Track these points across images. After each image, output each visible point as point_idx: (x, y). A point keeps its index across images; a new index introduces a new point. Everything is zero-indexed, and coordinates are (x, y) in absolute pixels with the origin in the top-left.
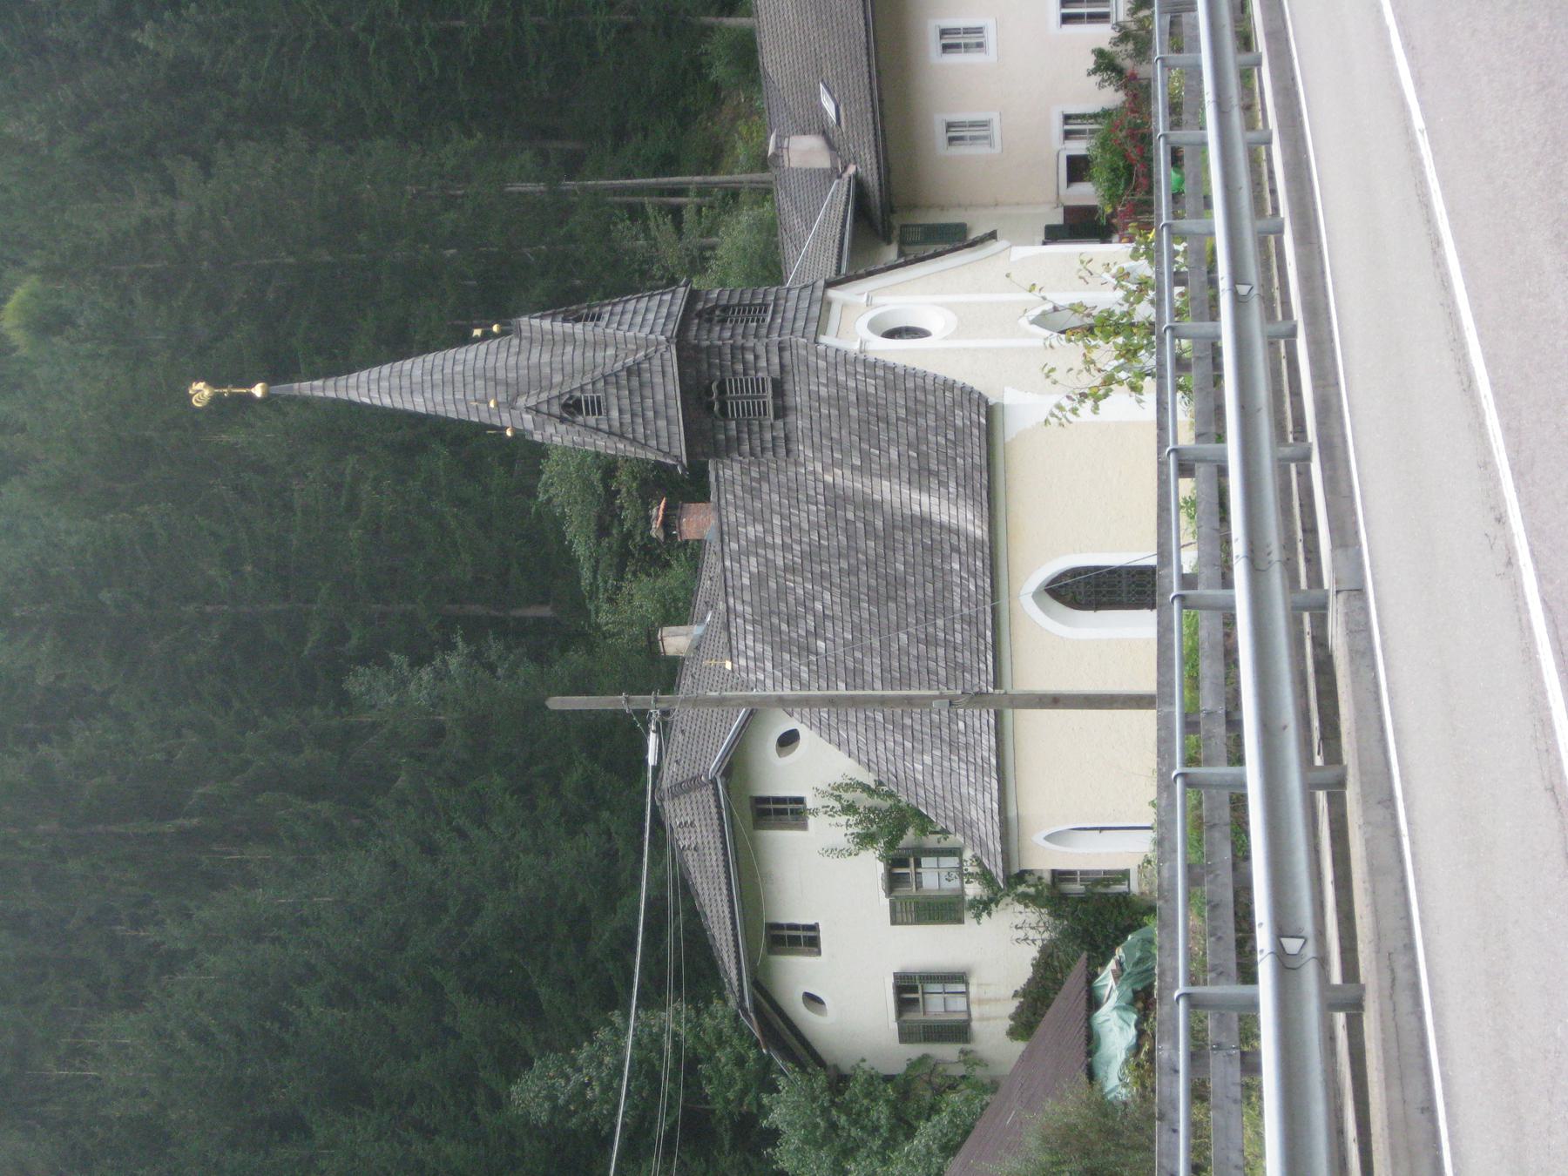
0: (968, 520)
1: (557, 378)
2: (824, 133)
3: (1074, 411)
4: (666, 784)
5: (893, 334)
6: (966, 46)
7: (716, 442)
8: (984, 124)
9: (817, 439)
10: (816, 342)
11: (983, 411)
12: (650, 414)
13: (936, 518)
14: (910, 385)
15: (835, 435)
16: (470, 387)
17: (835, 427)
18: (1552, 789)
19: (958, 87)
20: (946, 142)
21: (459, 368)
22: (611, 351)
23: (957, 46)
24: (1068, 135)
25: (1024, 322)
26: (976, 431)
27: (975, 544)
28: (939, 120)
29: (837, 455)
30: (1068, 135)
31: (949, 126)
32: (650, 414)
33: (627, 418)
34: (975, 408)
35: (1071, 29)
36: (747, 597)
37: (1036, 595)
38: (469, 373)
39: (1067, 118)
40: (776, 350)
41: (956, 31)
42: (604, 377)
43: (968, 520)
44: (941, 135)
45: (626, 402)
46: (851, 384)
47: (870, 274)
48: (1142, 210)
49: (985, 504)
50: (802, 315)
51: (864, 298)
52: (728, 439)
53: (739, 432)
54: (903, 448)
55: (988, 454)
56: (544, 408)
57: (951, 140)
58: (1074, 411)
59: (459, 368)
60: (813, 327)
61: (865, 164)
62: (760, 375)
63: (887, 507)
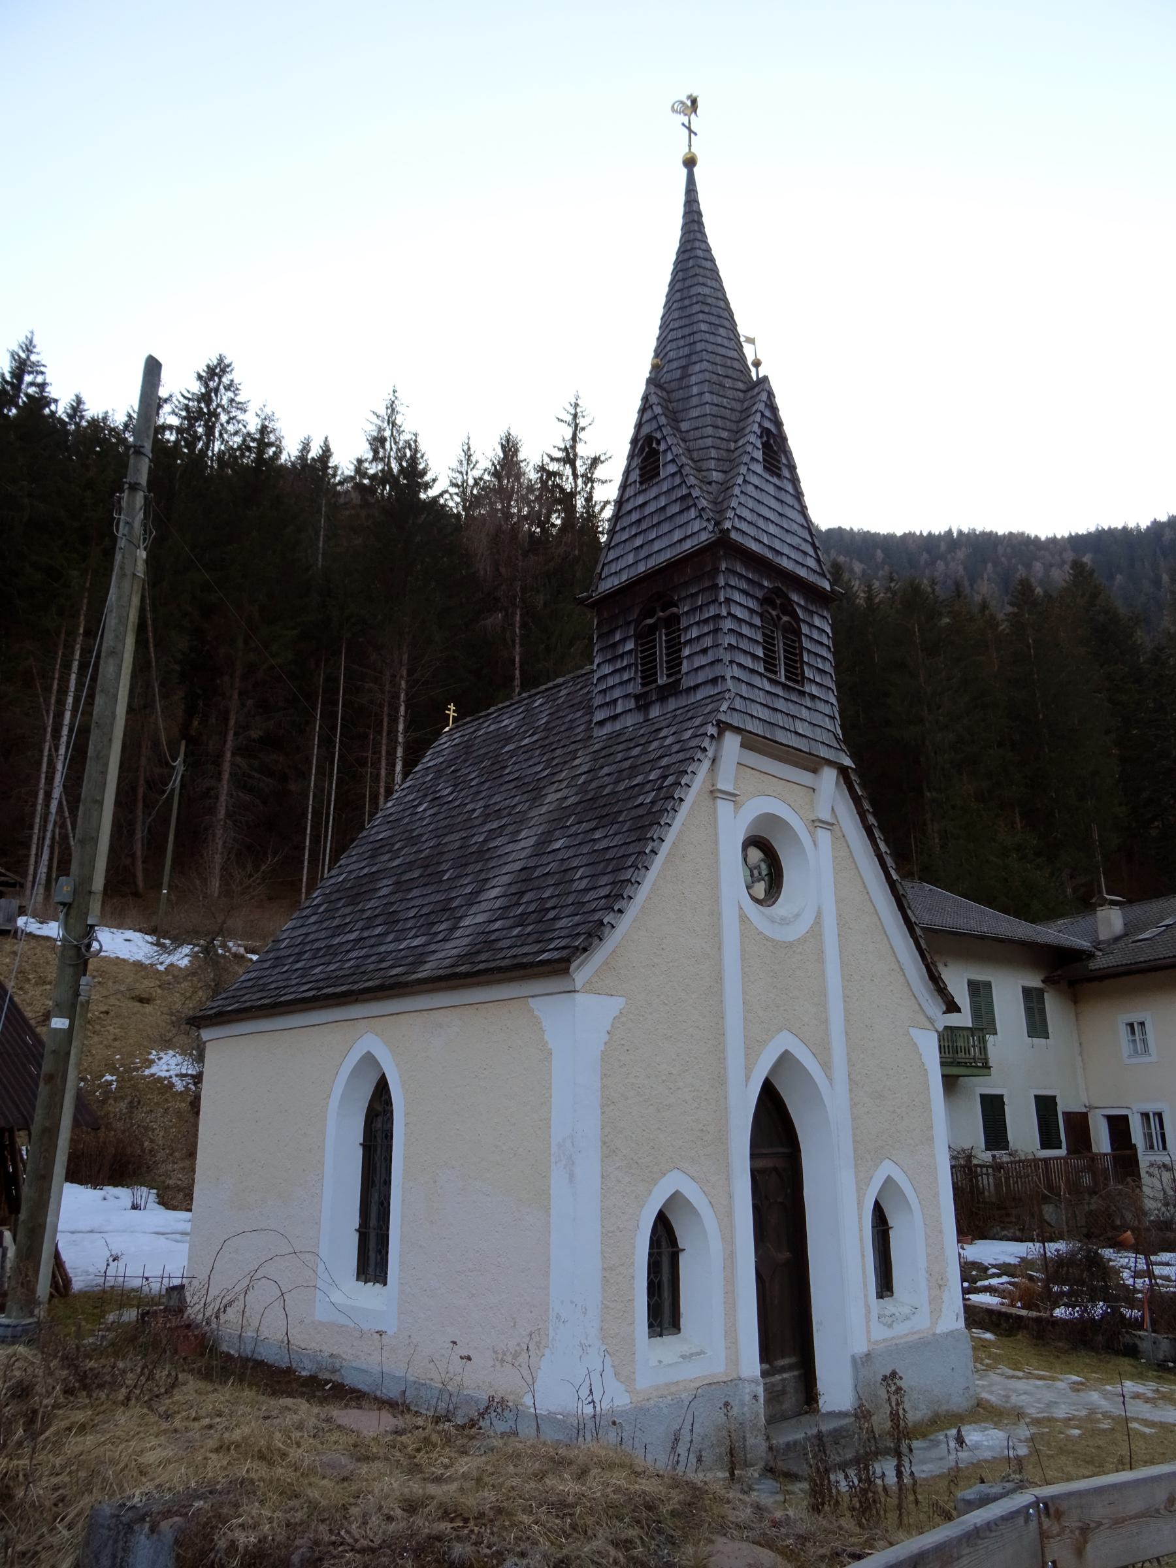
2: (1126, 935)
3: (480, 1428)
4: (104, 649)
6: (1134, 1041)
7: (612, 632)
8: (1146, 1051)
12: (638, 542)
16: (681, 343)
18: (91, 1232)
20: (1130, 1021)
21: (703, 327)
22: (715, 476)
23: (1133, 1033)
24: (1145, 1116)
30: (1145, 1116)
31: (1142, 1024)
32: (638, 542)
33: (635, 516)
36: (492, 728)
39: (1159, 1115)
41: (1144, 1033)
44: (1135, 1017)
51: (826, 816)
52: (614, 645)
53: (622, 656)
55: (500, 969)
57: (1131, 1025)
58: (480, 1428)
60: (751, 726)
61: (1101, 962)
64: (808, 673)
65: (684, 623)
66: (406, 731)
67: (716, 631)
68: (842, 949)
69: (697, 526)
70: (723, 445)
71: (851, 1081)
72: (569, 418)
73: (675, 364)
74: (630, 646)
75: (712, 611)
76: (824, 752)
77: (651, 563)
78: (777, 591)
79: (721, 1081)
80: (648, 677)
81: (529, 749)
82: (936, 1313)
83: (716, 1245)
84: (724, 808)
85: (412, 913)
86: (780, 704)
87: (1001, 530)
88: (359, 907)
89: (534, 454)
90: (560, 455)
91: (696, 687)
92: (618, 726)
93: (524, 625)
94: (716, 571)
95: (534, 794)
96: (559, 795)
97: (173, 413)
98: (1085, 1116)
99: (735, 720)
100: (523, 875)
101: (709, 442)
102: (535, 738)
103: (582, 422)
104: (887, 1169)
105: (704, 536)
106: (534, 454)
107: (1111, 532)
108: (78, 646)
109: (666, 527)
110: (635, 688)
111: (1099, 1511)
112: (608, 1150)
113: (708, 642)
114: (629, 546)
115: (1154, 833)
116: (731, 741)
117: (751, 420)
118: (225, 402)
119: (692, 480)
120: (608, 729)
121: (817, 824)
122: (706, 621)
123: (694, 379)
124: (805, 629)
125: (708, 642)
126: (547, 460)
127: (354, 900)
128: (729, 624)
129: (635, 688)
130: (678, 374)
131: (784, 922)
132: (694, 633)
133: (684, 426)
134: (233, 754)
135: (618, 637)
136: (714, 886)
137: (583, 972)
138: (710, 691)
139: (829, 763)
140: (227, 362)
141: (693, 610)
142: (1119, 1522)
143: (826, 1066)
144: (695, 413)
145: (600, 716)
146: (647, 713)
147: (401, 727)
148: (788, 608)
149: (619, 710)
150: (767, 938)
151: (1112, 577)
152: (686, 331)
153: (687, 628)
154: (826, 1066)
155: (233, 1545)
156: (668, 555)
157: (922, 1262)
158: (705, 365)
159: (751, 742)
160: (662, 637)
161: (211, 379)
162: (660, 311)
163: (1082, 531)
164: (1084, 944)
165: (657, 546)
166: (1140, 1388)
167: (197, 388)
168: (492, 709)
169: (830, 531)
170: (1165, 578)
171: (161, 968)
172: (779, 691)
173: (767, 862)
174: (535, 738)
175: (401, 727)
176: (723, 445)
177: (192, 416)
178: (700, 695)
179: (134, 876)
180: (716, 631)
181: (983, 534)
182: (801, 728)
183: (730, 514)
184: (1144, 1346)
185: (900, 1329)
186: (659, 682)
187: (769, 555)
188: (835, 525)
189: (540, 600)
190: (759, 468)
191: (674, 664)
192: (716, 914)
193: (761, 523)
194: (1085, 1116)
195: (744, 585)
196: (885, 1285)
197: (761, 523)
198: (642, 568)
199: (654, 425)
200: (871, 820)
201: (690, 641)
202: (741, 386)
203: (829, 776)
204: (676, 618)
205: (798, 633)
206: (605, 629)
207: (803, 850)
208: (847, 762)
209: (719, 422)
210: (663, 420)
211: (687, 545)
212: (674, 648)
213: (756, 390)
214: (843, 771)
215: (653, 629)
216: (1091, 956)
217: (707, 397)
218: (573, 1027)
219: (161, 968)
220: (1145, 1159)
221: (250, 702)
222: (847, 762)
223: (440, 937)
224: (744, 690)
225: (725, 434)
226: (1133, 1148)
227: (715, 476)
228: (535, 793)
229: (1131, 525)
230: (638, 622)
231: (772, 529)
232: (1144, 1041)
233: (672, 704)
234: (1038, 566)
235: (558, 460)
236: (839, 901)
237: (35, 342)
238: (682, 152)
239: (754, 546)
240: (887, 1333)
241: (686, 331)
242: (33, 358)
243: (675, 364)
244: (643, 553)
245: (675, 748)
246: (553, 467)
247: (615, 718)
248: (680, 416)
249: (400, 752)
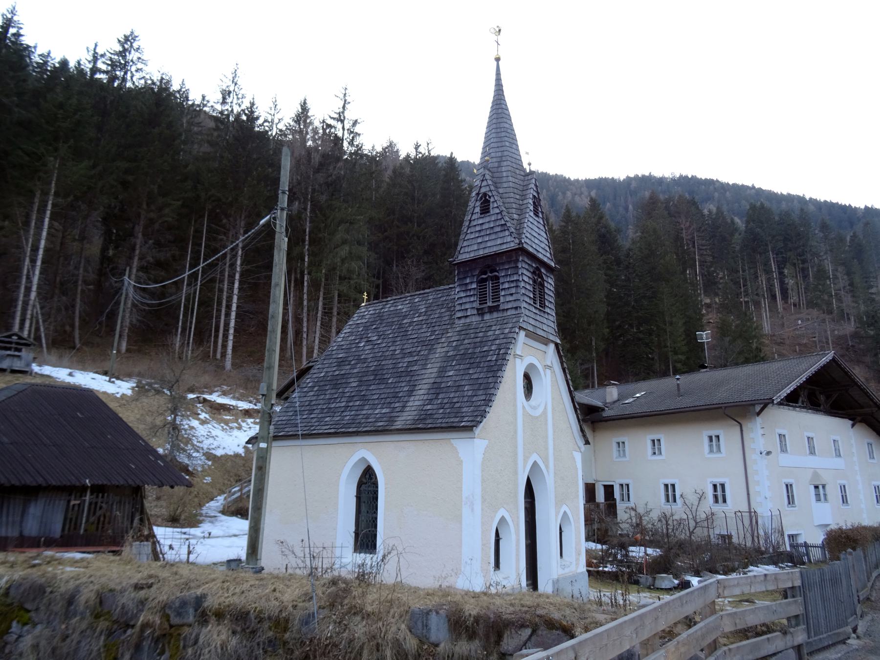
0: (405, 418)
1: (501, 191)
5: (527, 377)
7: (465, 278)
8: (624, 455)
9: (463, 332)
10: (521, 328)
11: (468, 424)
12: (480, 240)
13: (412, 398)
14: (490, 380)
15: (466, 341)
16: (497, 150)
17: (470, 341)
19: (638, 442)
21: (507, 144)
22: (515, 216)
23: (654, 445)
24: (622, 485)
25: (535, 457)
26: (457, 420)
27: (392, 420)
28: (625, 439)
29: (454, 344)
30: (622, 485)
31: (623, 443)
32: (480, 240)
33: (478, 228)
34: (470, 419)
35: (662, 488)
36: (392, 309)
37: (363, 460)
38: (504, 148)
39: (628, 485)
40: (515, 305)
42: (501, 213)
43: (405, 418)
44: (620, 440)
45: (486, 226)
46: (493, 348)
47: (560, 357)
48: (629, 576)
49: (413, 426)
50: (537, 324)
51: (549, 364)
52: (466, 284)
53: (470, 290)
54: (454, 378)
55: (442, 428)
56: (484, 183)
57: (619, 443)
59: (507, 144)
60: (531, 328)
61: (608, 413)
62: (502, 298)
63: (423, 372)
64: (547, 304)
65: (501, 280)
66: (241, 265)
67: (517, 286)
68: (553, 418)
69: (509, 239)
70: (517, 202)
71: (555, 473)
72: (342, 96)
73: (494, 160)
74: (474, 286)
75: (515, 278)
76: (552, 338)
77: (487, 251)
78: (537, 268)
79: (516, 473)
80: (483, 301)
81: (420, 323)
82: (577, 564)
83: (514, 537)
84: (518, 361)
85: (375, 397)
86: (538, 318)
87: (552, 172)
88: (341, 390)
89: (319, 114)
90: (336, 116)
91: (507, 309)
92: (468, 320)
93: (313, 211)
94: (517, 260)
95: (429, 347)
96: (444, 350)
97: (104, 63)
98: (594, 485)
99: (524, 325)
100: (436, 386)
101: (512, 200)
102: (421, 318)
103: (348, 99)
104: (564, 508)
105: (512, 244)
106: (319, 114)
107: (606, 179)
108: (50, 202)
109: (493, 237)
110: (476, 305)
111: (726, 584)
112: (484, 500)
113: (513, 291)
114: (474, 241)
115: (620, 342)
116: (522, 334)
117: (529, 191)
118: (135, 59)
119: (507, 219)
120: (463, 321)
121: (547, 367)
122: (512, 281)
123: (504, 169)
124: (546, 284)
125: (513, 291)
126: (327, 117)
127: (336, 386)
128: (522, 284)
129: (476, 305)
130: (496, 165)
131: (534, 408)
132: (506, 286)
133: (501, 191)
134: (138, 271)
135: (468, 281)
136: (515, 394)
137: (477, 431)
138: (513, 312)
139: (552, 341)
140: (136, 34)
141: (507, 275)
142: (730, 586)
143: (547, 467)
144: (505, 185)
145: (459, 315)
146: (483, 317)
147: (239, 262)
148: (540, 276)
149: (469, 314)
151: (604, 203)
152: (499, 144)
153: (503, 283)
154: (547, 467)
155: (470, 615)
156: (495, 249)
157: (574, 545)
158: (509, 163)
160: (490, 284)
161: (126, 43)
162: (484, 130)
163: (592, 178)
164: (599, 404)
165: (489, 244)
166: (644, 595)
167: (119, 48)
168: (389, 299)
169: (463, 162)
170: (631, 207)
171: (118, 396)
172: (537, 312)
174: (421, 318)
175: (239, 262)
176: (517, 202)
177: (113, 65)
178: (509, 313)
179: (74, 338)
180: (517, 286)
181: (542, 173)
183: (523, 236)
184: (642, 580)
185: (567, 570)
186: (489, 305)
187: (535, 253)
188: (465, 160)
189: (323, 198)
190: (532, 214)
191: (496, 298)
192: (515, 405)
193: (533, 239)
194: (594, 485)
195: (527, 267)
196: (497, 565)
197: (533, 239)
198: (481, 252)
199: (488, 189)
200: (565, 365)
201: (504, 289)
202: (522, 173)
203: (552, 347)
204: (497, 278)
205: (543, 286)
206: (461, 276)
207: (541, 379)
208: (559, 341)
209: (516, 191)
210: (492, 188)
211: (504, 247)
212: (496, 291)
213: (530, 177)
214: (557, 345)
215: (485, 280)
216: (603, 410)
217: (511, 179)
218: (470, 453)
219: (118, 396)
220: (621, 506)
221: (151, 242)
222: (559, 341)
223: (397, 410)
224: (527, 313)
225: (518, 197)
226: (615, 500)
227: (515, 216)
228: (430, 346)
229: (616, 177)
230: (478, 276)
231: (536, 241)
232: (624, 451)
233: (495, 315)
234: (569, 194)
235: (334, 119)
236: (553, 399)
237: (16, 9)
238: (494, 55)
239: (531, 249)
240: (563, 572)
241: (499, 144)
242: (15, 18)
243: (494, 160)
244: (482, 246)
245: (502, 336)
246: (330, 122)
247: (466, 317)
248: (499, 185)
249: (237, 276)
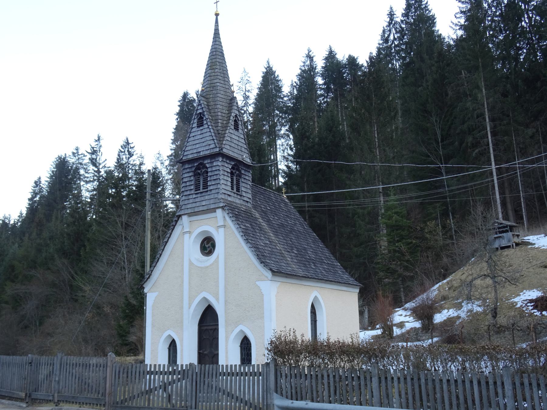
150: (199, 267)
159: (190, 215)
173: (208, 246)
182: (204, 203)
